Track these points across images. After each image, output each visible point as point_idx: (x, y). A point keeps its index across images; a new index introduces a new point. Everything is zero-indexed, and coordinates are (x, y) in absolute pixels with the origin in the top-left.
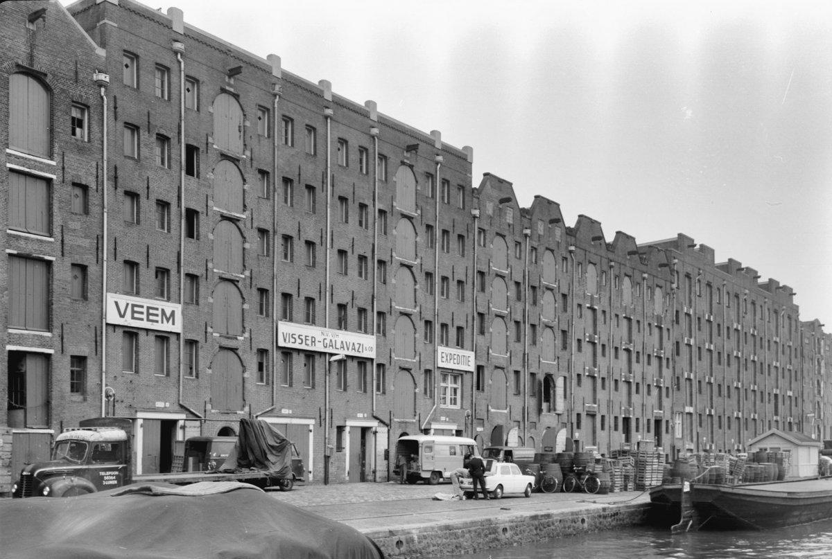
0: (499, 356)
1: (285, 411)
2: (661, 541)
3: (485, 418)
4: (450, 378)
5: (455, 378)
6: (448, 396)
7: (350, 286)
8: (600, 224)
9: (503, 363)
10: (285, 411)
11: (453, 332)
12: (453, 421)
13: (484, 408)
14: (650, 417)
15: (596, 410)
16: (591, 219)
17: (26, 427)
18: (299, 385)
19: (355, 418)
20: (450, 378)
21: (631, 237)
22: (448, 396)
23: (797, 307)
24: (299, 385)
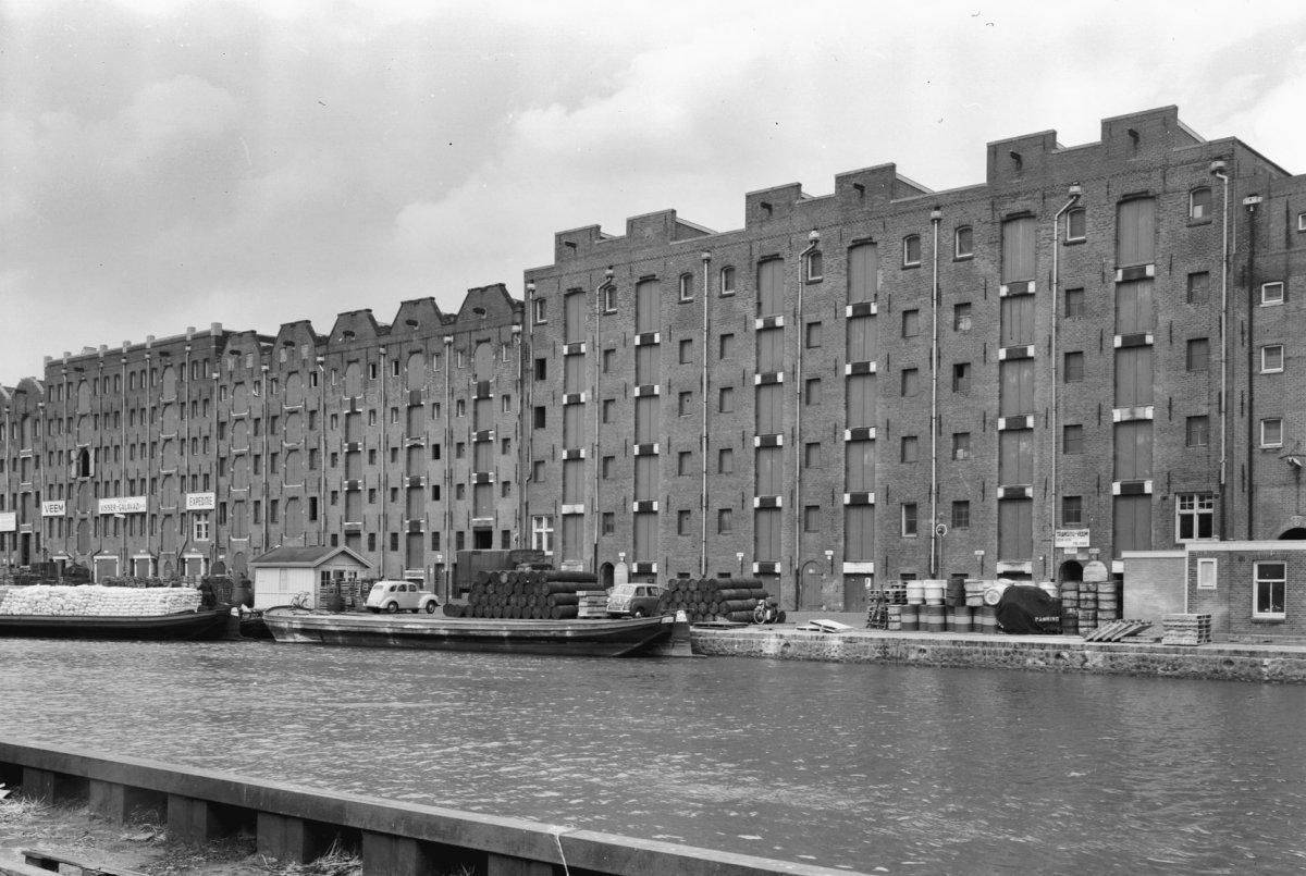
0: (239, 492)
1: (106, 552)
2: (954, 840)
3: (227, 546)
4: (203, 517)
5: (206, 515)
6: (203, 531)
7: (138, 466)
8: (1167, 116)
9: (243, 496)
10: (106, 552)
11: (200, 480)
12: (201, 551)
13: (226, 538)
14: (463, 528)
15: (493, 524)
16: (411, 302)
17: (1251, 538)
18: (111, 536)
19: (139, 553)
20: (203, 517)
21: (420, 300)
22: (203, 531)
23: (1108, 126)
24: (111, 536)
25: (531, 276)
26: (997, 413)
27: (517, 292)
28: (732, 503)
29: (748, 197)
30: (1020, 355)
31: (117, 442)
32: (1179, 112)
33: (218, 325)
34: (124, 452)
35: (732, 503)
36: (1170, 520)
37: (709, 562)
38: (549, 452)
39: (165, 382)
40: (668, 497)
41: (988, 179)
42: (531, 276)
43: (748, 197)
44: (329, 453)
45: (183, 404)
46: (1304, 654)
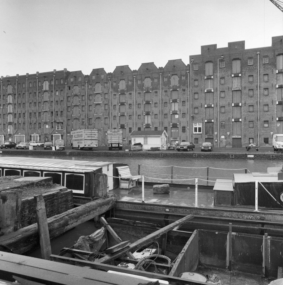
1: (35, 133)
19: (34, 134)
25: (191, 57)
26: (204, 104)
27: (187, 62)
28: (269, 119)
29: (273, 38)
30: (210, 91)
31: (24, 102)
32: (217, 46)
33: (65, 69)
34: (27, 105)
35: (269, 119)
36: (192, 129)
37: (261, 135)
38: (200, 105)
39: (8, 88)
40: (245, 117)
41: (272, 45)
42: (191, 57)
43: (273, 38)
44: (113, 105)
45: (15, 94)
46: (5, 154)
